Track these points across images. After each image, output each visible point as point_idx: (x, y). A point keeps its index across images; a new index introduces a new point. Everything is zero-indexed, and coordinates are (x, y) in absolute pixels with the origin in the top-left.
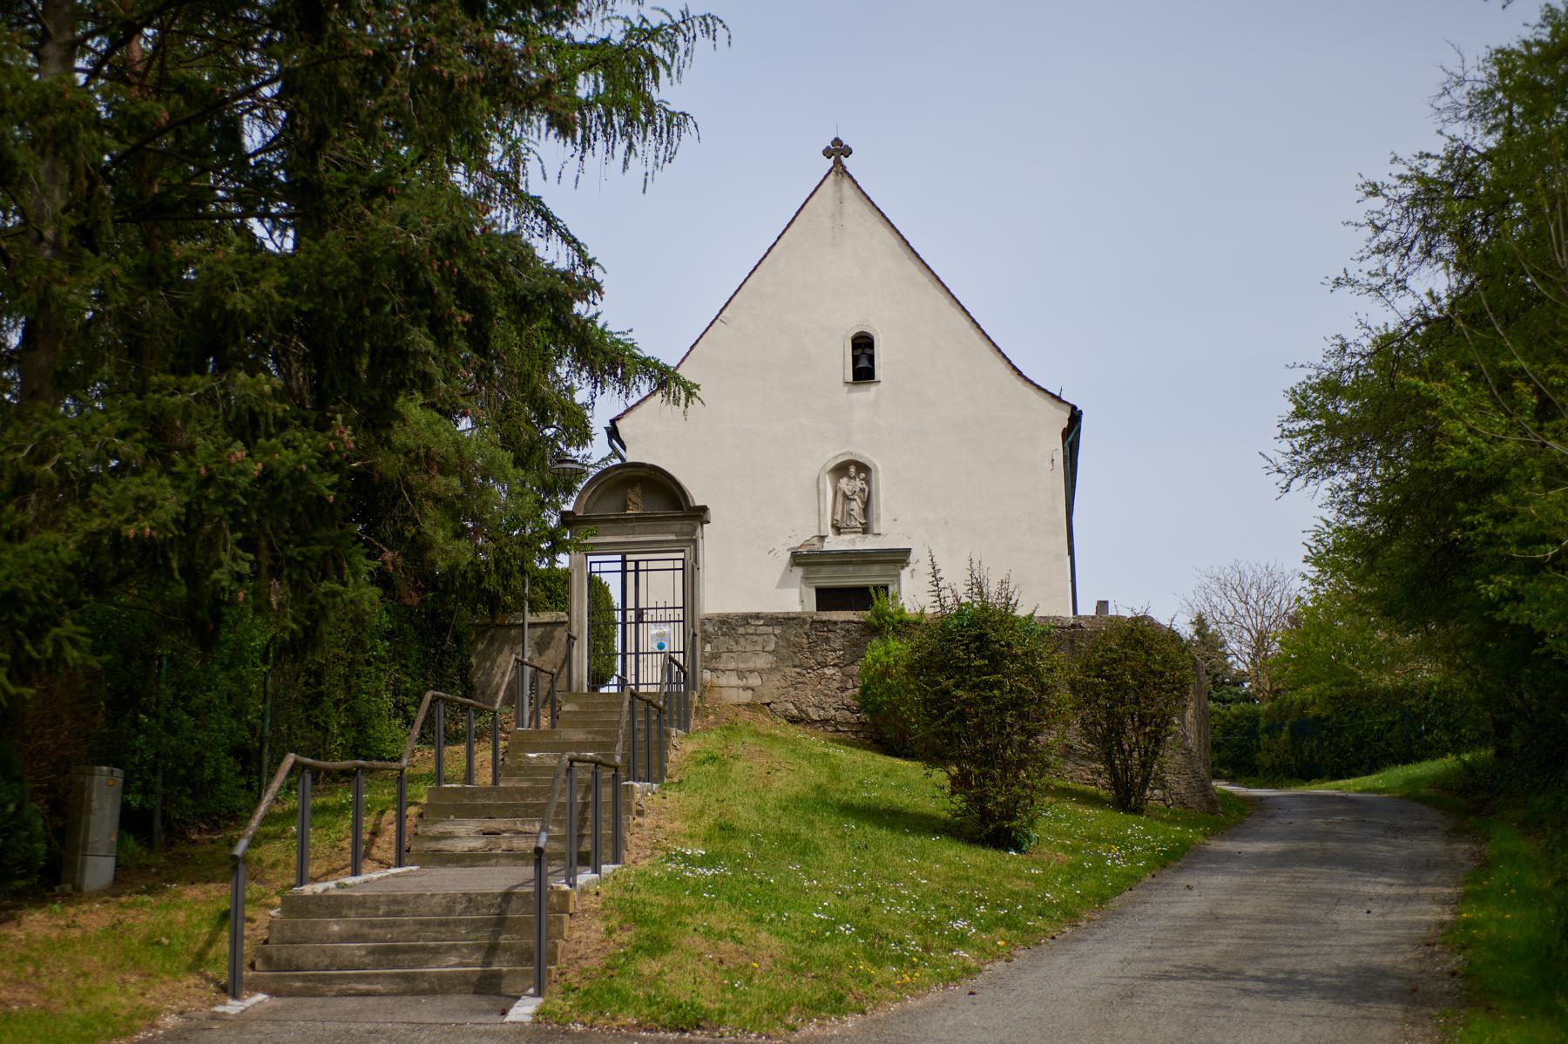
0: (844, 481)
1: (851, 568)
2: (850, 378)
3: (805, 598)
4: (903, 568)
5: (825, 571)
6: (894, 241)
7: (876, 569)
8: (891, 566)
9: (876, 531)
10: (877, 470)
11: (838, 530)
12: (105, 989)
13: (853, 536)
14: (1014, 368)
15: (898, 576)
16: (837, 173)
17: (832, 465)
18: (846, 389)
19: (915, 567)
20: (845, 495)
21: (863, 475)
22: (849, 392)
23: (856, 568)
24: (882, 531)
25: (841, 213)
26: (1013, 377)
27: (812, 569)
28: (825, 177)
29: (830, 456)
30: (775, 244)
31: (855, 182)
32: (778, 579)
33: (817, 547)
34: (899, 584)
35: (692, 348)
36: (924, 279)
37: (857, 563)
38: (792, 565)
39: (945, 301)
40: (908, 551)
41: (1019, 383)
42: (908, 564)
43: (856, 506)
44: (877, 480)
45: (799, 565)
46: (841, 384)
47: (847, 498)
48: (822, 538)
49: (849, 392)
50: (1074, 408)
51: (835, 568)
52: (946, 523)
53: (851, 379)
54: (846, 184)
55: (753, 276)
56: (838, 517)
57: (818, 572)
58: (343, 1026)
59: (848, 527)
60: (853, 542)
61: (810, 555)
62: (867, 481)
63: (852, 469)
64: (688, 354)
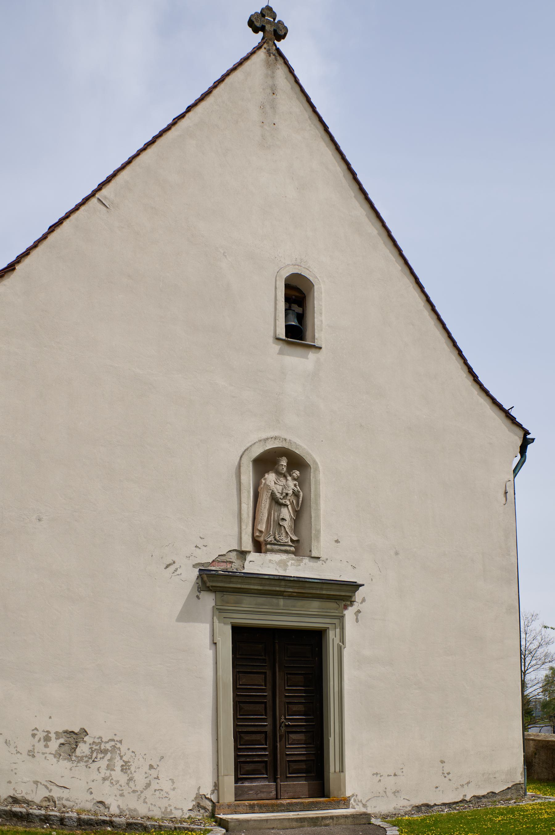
0: (271, 478)
1: (281, 602)
2: (282, 333)
3: (218, 639)
4: (346, 607)
5: (248, 602)
6: (339, 169)
7: (315, 606)
8: (332, 605)
9: (314, 554)
10: (317, 469)
11: (258, 547)
12: (458, 777)
13: (284, 557)
14: (470, 370)
15: (342, 618)
16: (269, 52)
17: (257, 451)
18: (277, 347)
19: (362, 607)
20: (273, 498)
21: (296, 473)
22: (281, 353)
23: (289, 602)
24: (323, 556)
25: (273, 107)
26: (468, 381)
27: (232, 597)
28: (253, 53)
29: (255, 437)
30: (182, 116)
31: (291, 71)
32: (179, 607)
33: (235, 566)
34: (342, 629)
35: (52, 229)
36: (373, 229)
37: (291, 596)
38: (200, 590)
39: (397, 266)
40: (355, 586)
41: (475, 391)
42: (352, 603)
43: (286, 513)
44: (317, 483)
45: (209, 589)
46: (271, 340)
47: (276, 502)
48: (243, 554)
49: (281, 353)
50: (526, 433)
51: (261, 600)
52: (397, 554)
53: (283, 336)
54: (281, 72)
55: (149, 151)
56: (262, 527)
57: (238, 603)
58: (278, 543)
59: (277, 543)
60: (283, 564)
61: (230, 576)
62: (301, 482)
63: (284, 462)
64: (45, 237)
